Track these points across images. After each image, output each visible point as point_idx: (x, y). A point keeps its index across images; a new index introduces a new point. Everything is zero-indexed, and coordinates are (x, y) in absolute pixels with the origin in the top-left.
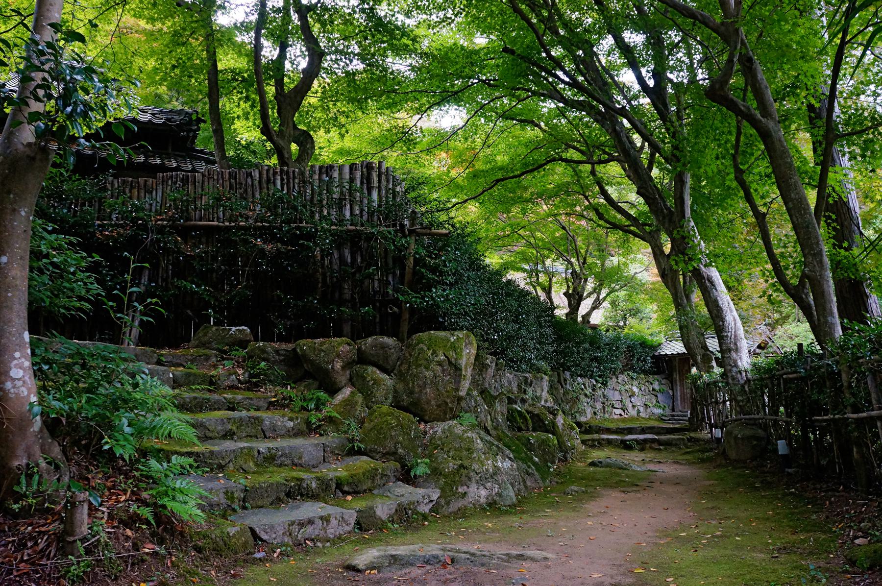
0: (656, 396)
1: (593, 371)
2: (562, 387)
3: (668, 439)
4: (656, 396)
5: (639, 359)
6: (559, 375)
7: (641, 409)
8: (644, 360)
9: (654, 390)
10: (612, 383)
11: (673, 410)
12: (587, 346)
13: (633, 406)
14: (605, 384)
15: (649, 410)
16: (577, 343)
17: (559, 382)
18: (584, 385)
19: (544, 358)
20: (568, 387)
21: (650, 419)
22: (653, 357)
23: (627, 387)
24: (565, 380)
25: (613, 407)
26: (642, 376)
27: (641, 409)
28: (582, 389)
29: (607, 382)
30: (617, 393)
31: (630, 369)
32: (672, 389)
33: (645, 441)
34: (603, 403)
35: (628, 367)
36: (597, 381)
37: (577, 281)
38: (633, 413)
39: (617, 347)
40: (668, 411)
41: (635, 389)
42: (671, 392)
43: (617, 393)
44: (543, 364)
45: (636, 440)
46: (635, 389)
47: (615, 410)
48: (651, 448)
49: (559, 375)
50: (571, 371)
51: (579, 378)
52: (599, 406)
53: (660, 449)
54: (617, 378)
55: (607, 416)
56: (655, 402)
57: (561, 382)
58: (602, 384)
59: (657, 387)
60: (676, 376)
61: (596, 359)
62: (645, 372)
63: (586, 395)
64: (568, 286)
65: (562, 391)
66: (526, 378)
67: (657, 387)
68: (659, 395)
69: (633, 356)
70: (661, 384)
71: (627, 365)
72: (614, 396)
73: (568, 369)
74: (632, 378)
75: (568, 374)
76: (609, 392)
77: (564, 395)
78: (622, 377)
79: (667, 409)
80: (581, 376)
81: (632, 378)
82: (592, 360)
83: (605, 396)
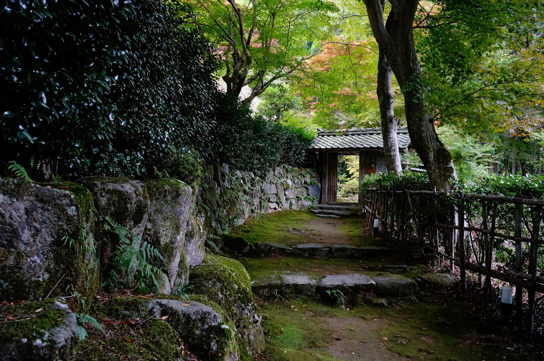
0: (307, 189)
1: (253, 163)
2: (219, 185)
3: (393, 285)
4: (307, 189)
5: (295, 152)
6: (216, 170)
7: (294, 202)
8: (300, 154)
9: (305, 183)
10: (270, 175)
11: (320, 202)
12: (250, 132)
13: (287, 199)
14: (263, 177)
15: (300, 203)
16: (239, 127)
17: (216, 179)
18: (243, 179)
19: (192, 141)
20: (226, 184)
21: (300, 211)
22: (308, 150)
23: (282, 180)
24: (223, 175)
25: (269, 201)
26: (296, 169)
27: (294, 202)
28: (241, 185)
29: (265, 175)
30: (273, 186)
31: (285, 162)
32: (321, 182)
33: (357, 288)
34: (260, 198)
35: (286, 160)
36: (255, 174)
37: (239, 64)
38: (286, 205)
39: (278, 138)
40: (316, 204)
41: (290, 182)
42: (319, 185)
43: (273, 186)
44: (189, 155)
45: (341, 288)
46: (290, 182)
47: (270, 204)
48: (369, 302)
49: (216, 170)
50: (230, 164)
51: (238, 172)
52: (256, 202)
53: (382, 305)
54: (274, 170)
55: (263, 212)
56: (305, 195)
57: (218, 178)
58: (261, 177)
59: (308, 180)
60: (326, 170)
61: (259, 150)
62: (299, 165)
63: (245, 192)
64: (228, 71)
65: (218, 192)
66: (123, 197)
67: (308, 180)
68: (310, 188)
69: (290, 148)
70: (312, 177)
71: (283, 158)
72: (271, 190)
73: (228, 161)
74: (287, 171)
75: (226, 167)
76: (266, 186)
77: (221, 196)
78: (279, 170)
79: (315, 201)
80: (240, 169)
81: (287, 171)
82: (253, 150)
83: (262, 191)
